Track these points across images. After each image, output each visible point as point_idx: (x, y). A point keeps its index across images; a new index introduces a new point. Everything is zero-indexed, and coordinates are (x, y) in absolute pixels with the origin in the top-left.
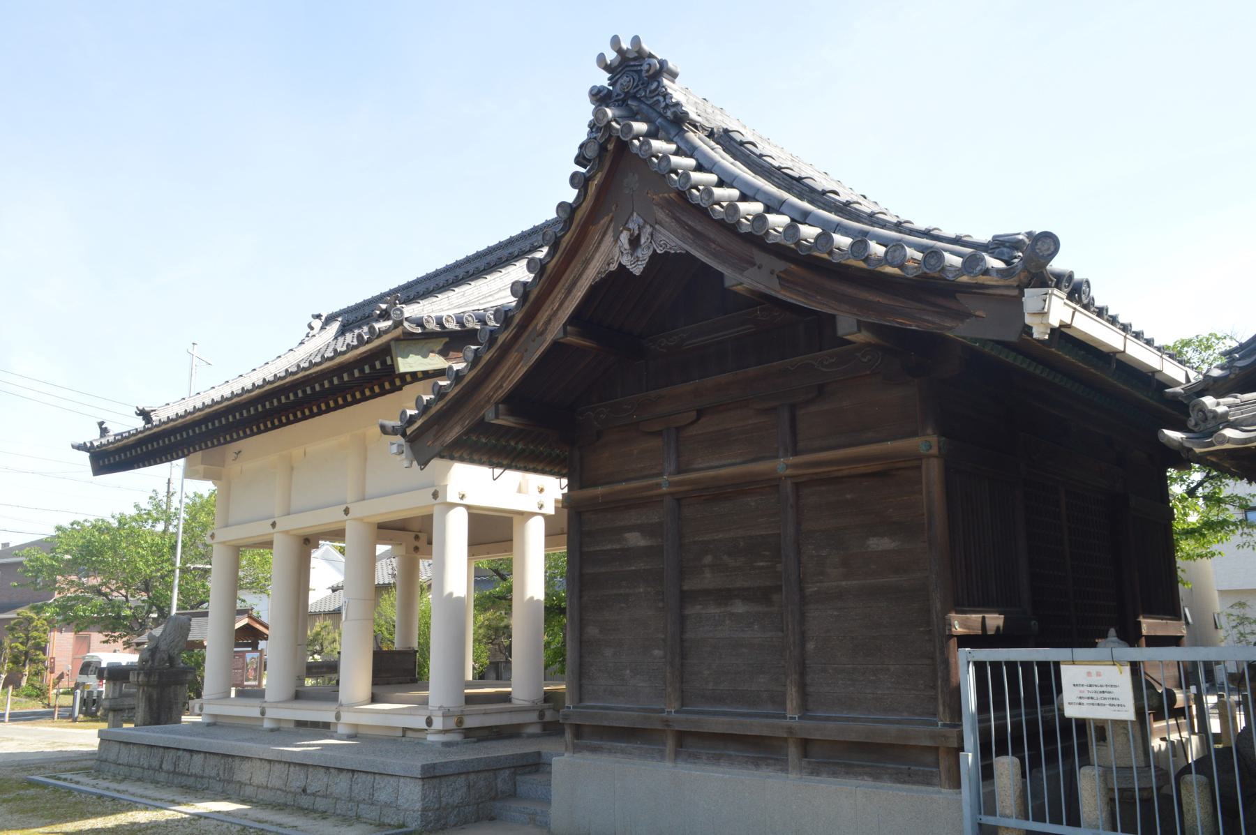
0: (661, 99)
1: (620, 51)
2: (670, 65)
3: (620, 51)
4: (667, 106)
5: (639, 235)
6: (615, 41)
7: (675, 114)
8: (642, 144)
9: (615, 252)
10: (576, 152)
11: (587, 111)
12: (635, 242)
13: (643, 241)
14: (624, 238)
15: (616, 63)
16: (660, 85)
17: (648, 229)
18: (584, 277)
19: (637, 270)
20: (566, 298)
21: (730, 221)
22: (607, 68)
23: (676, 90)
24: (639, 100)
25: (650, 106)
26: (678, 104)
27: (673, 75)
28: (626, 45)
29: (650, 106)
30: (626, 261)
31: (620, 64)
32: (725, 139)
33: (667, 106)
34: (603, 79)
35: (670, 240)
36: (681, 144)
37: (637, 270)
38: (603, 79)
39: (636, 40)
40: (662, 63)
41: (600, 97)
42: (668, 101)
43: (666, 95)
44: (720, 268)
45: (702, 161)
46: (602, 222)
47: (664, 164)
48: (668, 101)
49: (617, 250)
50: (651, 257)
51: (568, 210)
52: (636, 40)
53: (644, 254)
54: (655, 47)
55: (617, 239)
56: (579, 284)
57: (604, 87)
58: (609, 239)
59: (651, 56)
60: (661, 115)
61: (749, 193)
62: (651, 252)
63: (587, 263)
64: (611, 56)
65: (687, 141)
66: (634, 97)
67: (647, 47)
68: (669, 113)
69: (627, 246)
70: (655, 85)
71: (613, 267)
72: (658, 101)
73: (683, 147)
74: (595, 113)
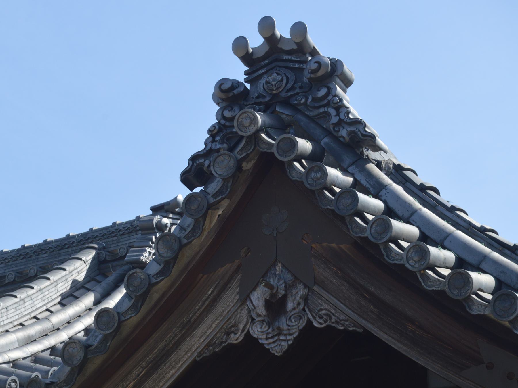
0: (333, 112)
1: (271, 39)
2: (347, 68)
3: (271, 39)
4: (341, 123)
5: (284, 298)
6: (266, 25)
7: (352, 134)
8: (309, 171)
9: (238, 315)
10: (184, 165)
11: (209, 114)
12: (275, 307)
13: (290, 306)
14: (258, 297)
15: (261, 54)
16: (330, 91)
17: (301, 291)
18: (184, 347)
19: (278, 347)
20: (148, 375)
21: (455, 294)
22: (247, 58)
23: (355, 102)
24: (295, 108)
25: (312, 119)
26: (358, 122)
27: (347, 82)
28: (283, 31)
29: (312, 119)
30: (257, 331)
31: (267, 55)
32: (398, 172)
33: (341, 123)
34: (237, 71)
35: (335, 310)
36: (359, 177)
37: (278, 347)
38: (237, 71)
39: (299, 29)
40: (336, 64)
41: (228, 94)
42: (342, 116)
43: (340, 107)
44: (421, 361)
45: (392, 205)
46: (221, 271)
47: (346, 202)
48: (342, 116)
49: (244, 313)
50: (302, 332)
51: (176, 246)
52: (299, 29)
53: (291, 327)
54: (326, 45)
55: (245, 298)
56: (173, 357)
57: (239, 83)
58: (231, 297)
59: (314, 52)
60: (328, 133)
61: (469, 258)
62: (303, 323)
63: (190, 327)
64: (256, 41)
65: (370, 175)
66: (286, 103)
67: (314, 39)
68: (344, 133)
69: (261, 310)
70: (323, 92)
71: (236, 338)
72: (328, 114)
73: (364, 182)
74: (220, 115)
